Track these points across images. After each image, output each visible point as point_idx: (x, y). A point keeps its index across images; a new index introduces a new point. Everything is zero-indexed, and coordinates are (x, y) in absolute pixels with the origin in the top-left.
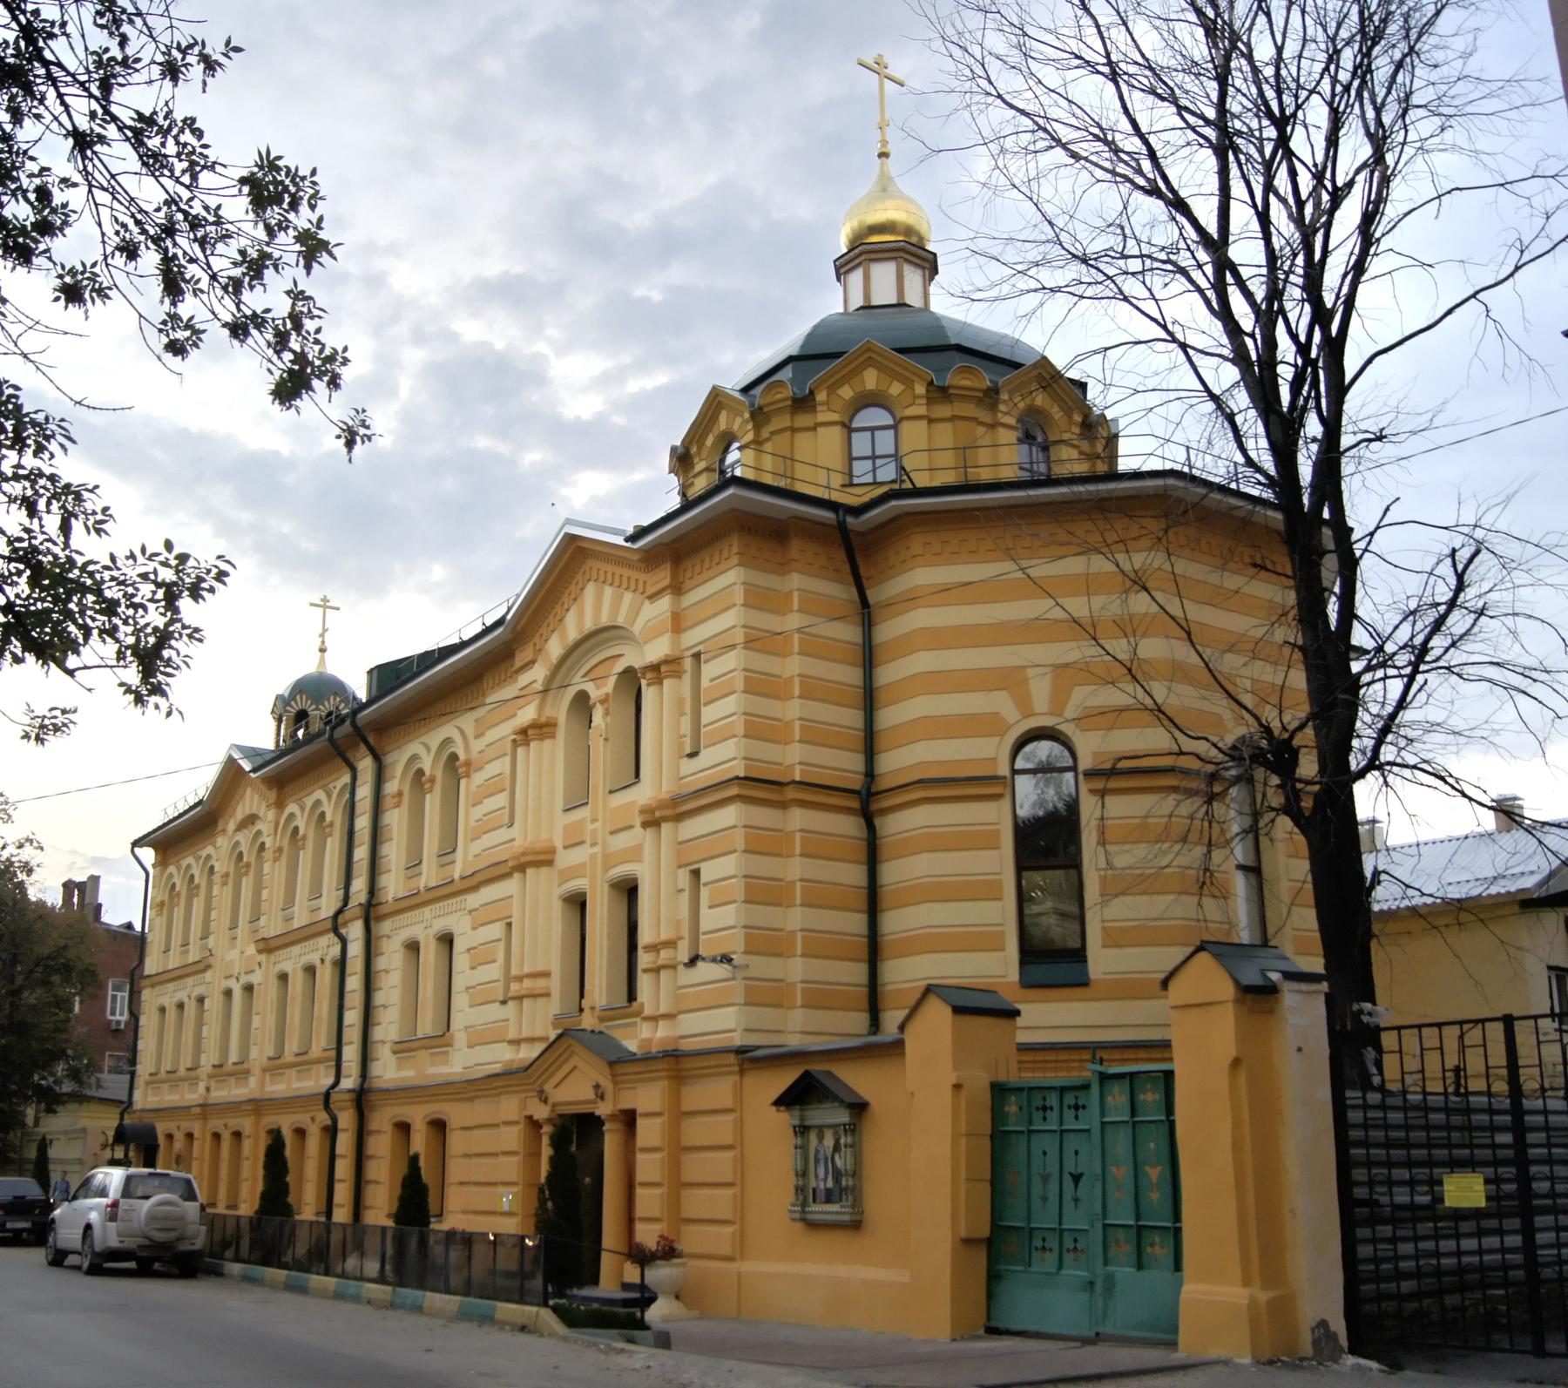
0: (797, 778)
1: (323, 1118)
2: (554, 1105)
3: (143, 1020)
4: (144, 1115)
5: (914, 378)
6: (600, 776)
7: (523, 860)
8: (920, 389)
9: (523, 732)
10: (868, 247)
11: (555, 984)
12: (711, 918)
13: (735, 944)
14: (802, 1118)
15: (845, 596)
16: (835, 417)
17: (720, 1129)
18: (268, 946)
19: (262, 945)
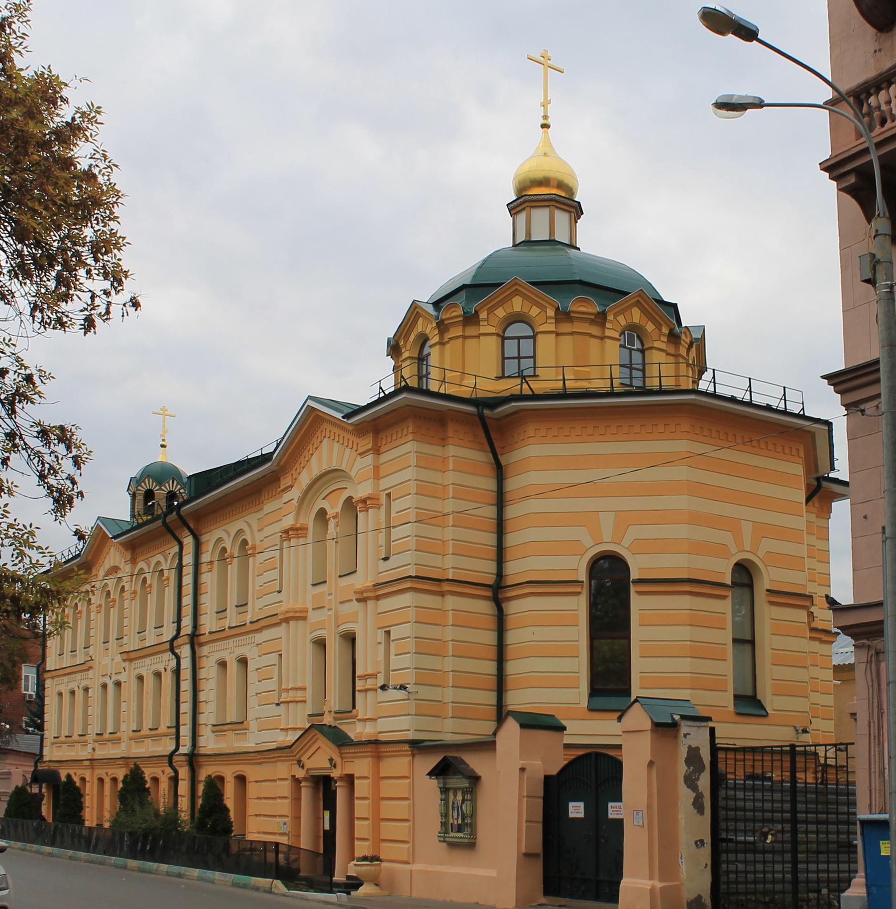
0: (450, 578)
1: (169, 771)
3: (47, 701)
4: (51, 764)
6: (332, 568)
7: (288, 615)
8: (551, 313)
9: (286, 532)
11: (309, 695)
12: (396, 662)
13: (409, 678)
14: (445, 783)
15: (485, 460)
16: (492, 330)
17: (400, 788)
18: (130, 657)
19: (125, 656)
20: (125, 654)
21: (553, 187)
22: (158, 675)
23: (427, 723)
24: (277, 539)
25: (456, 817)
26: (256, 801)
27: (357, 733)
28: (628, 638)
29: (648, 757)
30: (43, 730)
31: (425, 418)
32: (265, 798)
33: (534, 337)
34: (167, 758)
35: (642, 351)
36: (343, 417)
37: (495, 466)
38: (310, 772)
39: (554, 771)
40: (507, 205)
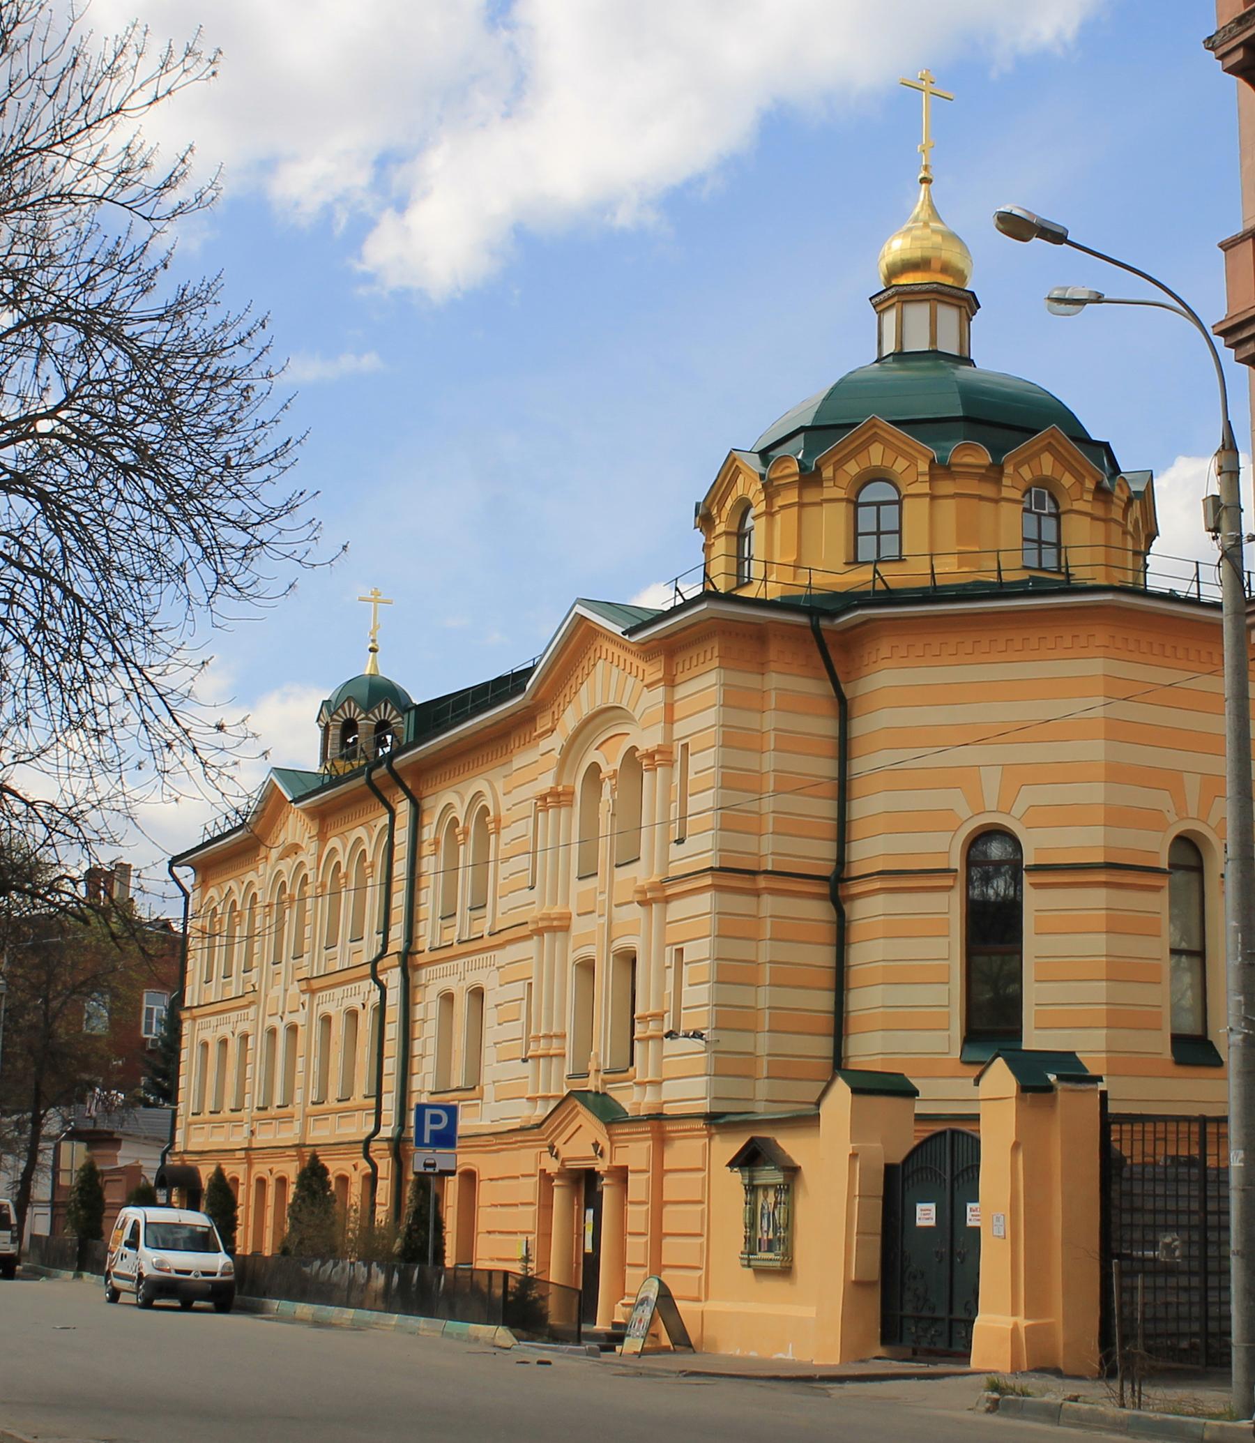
0: (770, 869)
1: (364, 1166)
2: (563, 1161)
5: (916, 454)
7: (541, 924)
8: (923, 467)
9: (543, 798)
10: (901, 289)
14: (751, 1178)
16: (841, 494)
19: (304, 985)
20: (304, 982)
21: (935, 271)
22: (352, 1015)
23: (734, 1087)
24: (528, 808)
25: (765, 1229)
26: (489, 1210)
27: (634, 1104)
28: (1020, 953)
29: (1011, 1137)
30: (177, 1103)
31: (737, 634)
32: (502, 1205)
33: (899, 503)
34: (361, 1145)
35: (1057, 516)
36: (623, 633)
37: (836, 700)
38: (567, 1163)
39: (898, 1158)
40: (871, 299)
